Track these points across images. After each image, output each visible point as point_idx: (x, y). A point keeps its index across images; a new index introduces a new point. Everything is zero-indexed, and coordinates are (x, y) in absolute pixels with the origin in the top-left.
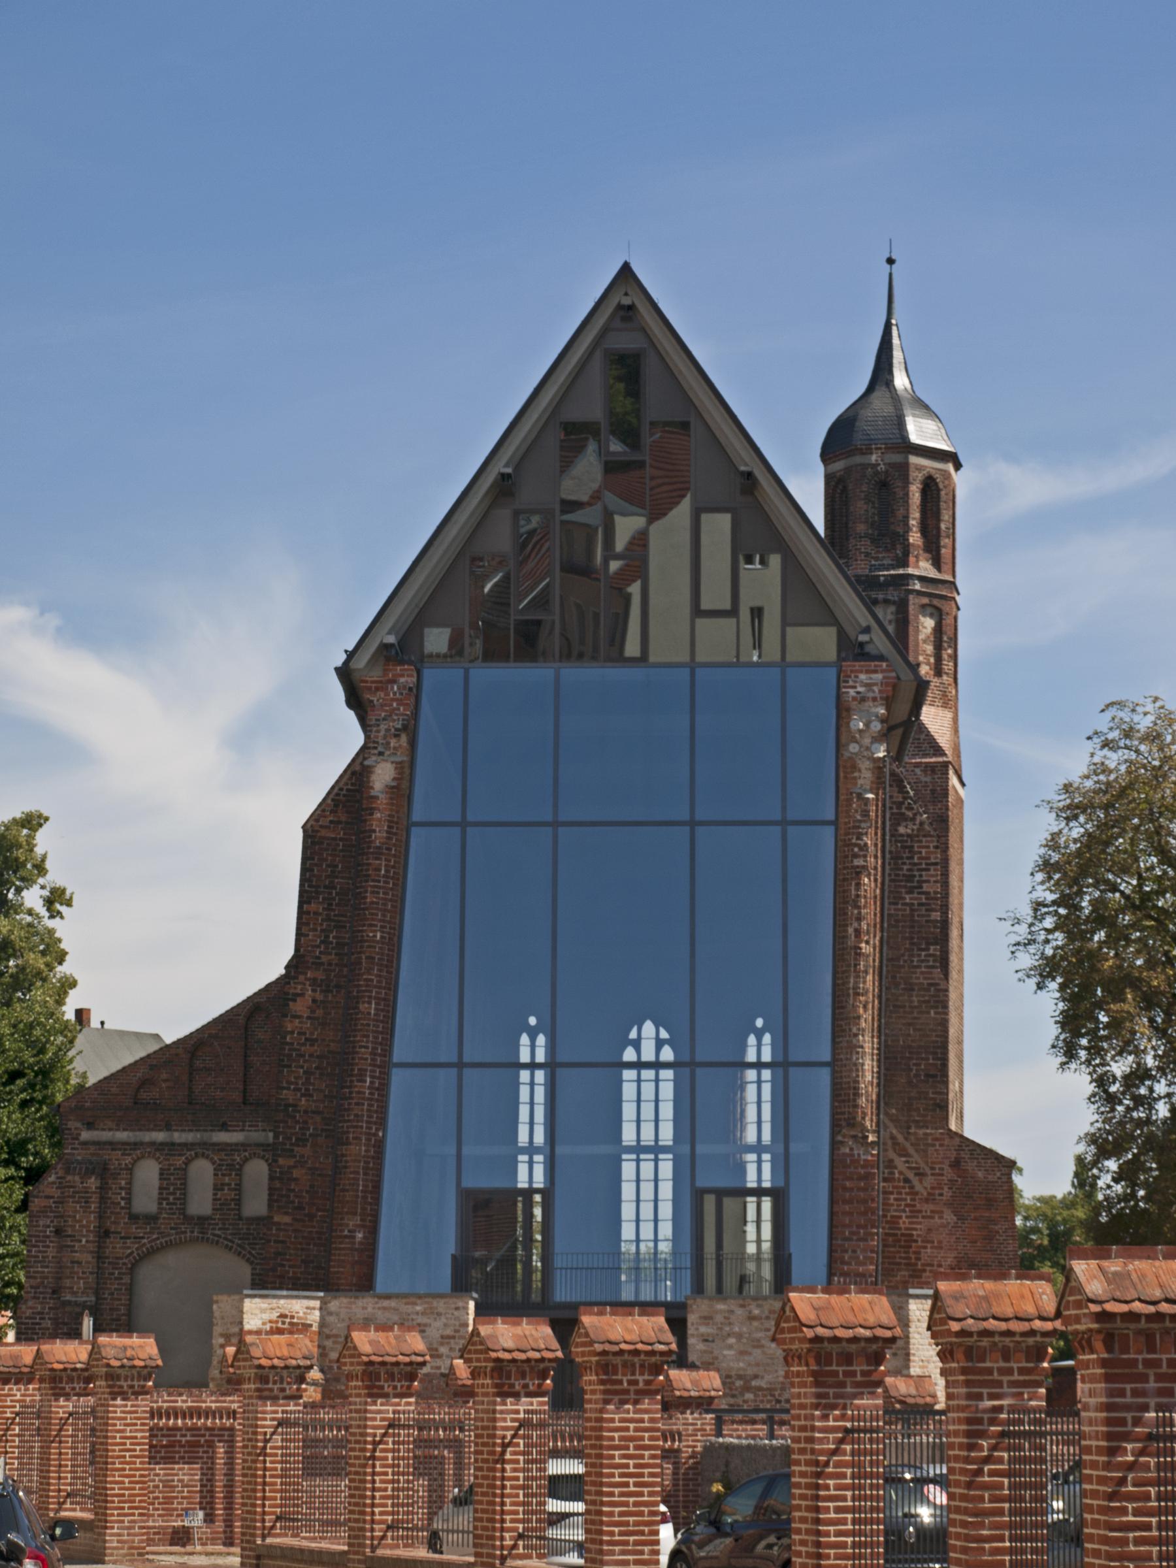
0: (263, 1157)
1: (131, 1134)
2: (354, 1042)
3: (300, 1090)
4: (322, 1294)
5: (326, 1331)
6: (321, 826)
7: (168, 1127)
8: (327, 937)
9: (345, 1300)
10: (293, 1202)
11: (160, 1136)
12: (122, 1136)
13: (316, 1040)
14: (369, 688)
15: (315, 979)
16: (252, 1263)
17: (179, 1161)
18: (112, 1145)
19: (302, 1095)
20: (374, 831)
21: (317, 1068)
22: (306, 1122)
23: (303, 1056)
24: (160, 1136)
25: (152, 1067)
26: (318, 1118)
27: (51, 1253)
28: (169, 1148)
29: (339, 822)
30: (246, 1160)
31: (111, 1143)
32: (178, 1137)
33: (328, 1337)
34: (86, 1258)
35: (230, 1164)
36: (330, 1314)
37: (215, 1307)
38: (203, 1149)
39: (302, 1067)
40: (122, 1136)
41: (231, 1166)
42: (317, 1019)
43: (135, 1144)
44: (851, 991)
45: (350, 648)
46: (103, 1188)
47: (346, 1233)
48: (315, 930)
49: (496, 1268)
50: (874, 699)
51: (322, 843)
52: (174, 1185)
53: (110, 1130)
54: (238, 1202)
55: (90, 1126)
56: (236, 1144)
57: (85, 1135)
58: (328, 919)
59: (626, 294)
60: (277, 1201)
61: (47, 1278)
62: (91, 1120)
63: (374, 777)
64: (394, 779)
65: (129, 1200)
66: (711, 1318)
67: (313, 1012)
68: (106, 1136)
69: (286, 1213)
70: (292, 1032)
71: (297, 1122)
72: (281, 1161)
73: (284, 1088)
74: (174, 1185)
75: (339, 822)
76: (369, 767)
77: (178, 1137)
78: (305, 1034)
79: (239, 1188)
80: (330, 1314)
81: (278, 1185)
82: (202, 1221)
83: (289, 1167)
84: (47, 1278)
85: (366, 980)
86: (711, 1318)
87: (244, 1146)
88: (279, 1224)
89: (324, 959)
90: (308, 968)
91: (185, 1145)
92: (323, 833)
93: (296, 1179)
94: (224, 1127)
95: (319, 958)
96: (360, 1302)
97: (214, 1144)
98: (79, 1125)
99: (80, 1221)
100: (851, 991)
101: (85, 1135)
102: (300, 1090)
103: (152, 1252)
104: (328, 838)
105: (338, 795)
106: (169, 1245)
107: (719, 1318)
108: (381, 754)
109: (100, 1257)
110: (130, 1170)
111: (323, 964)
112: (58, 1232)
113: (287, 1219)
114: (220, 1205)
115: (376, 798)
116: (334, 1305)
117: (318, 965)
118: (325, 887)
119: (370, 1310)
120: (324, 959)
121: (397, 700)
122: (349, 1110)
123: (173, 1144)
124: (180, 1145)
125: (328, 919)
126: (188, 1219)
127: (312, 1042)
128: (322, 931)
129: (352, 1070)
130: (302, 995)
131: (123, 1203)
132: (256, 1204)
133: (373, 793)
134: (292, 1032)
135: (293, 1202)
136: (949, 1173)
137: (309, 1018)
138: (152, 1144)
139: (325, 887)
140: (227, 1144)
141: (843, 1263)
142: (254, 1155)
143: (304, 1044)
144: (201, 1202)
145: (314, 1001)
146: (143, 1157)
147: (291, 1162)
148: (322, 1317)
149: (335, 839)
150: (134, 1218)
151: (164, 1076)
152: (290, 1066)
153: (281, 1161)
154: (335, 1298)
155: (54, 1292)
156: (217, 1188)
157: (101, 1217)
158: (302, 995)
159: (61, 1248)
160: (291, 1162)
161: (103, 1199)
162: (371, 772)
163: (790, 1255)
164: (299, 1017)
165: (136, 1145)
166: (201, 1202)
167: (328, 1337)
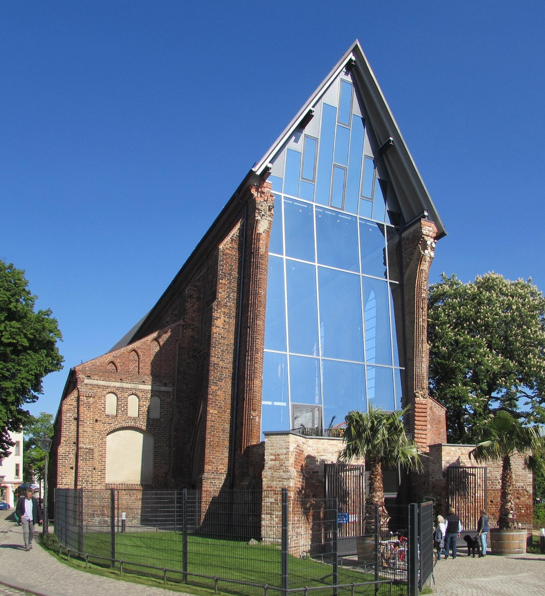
0: (158, 396)
3: (219, 358)
6: (226, 248)
11: (118, 384)
15: (225, 312)
18: (99, 386)
22: (222, 372)
23: (221, 344)
26: (227, 370)
29: (233, 248)
32: (125, 385)
39: (220, 348)
42: (226, 329)
48: (224, 291)
52: (122, 406)
61: (71, 437)
62: (89, 375)
64: (268, 228)
66: (449, 454)
71: (219, 371)
74: (122, 406)
75: (233, 248)
77: (125, 385)
84: (71, 437)
86: (449, 454)
88: (212, 413)
90: (223, 307)
92: (227, 251)
93: (219, 395)
98: (84, 377)
101: (87, 381)
102: (219, 358)
105: (233, 236)
107: (452, 453)
111: (228, 306)
113: (216, 412)
117: (225, 306)
120: (228, 304)
123: (123, 388)
124: (126, 388)
130: (220, 318)
134: (216, 333)
135: (217, 405)
137: (222, 328)
145: (224, 321)
150: (108, 416)
151: (119, 361)
158: (220, 318)
163: (14, 501)
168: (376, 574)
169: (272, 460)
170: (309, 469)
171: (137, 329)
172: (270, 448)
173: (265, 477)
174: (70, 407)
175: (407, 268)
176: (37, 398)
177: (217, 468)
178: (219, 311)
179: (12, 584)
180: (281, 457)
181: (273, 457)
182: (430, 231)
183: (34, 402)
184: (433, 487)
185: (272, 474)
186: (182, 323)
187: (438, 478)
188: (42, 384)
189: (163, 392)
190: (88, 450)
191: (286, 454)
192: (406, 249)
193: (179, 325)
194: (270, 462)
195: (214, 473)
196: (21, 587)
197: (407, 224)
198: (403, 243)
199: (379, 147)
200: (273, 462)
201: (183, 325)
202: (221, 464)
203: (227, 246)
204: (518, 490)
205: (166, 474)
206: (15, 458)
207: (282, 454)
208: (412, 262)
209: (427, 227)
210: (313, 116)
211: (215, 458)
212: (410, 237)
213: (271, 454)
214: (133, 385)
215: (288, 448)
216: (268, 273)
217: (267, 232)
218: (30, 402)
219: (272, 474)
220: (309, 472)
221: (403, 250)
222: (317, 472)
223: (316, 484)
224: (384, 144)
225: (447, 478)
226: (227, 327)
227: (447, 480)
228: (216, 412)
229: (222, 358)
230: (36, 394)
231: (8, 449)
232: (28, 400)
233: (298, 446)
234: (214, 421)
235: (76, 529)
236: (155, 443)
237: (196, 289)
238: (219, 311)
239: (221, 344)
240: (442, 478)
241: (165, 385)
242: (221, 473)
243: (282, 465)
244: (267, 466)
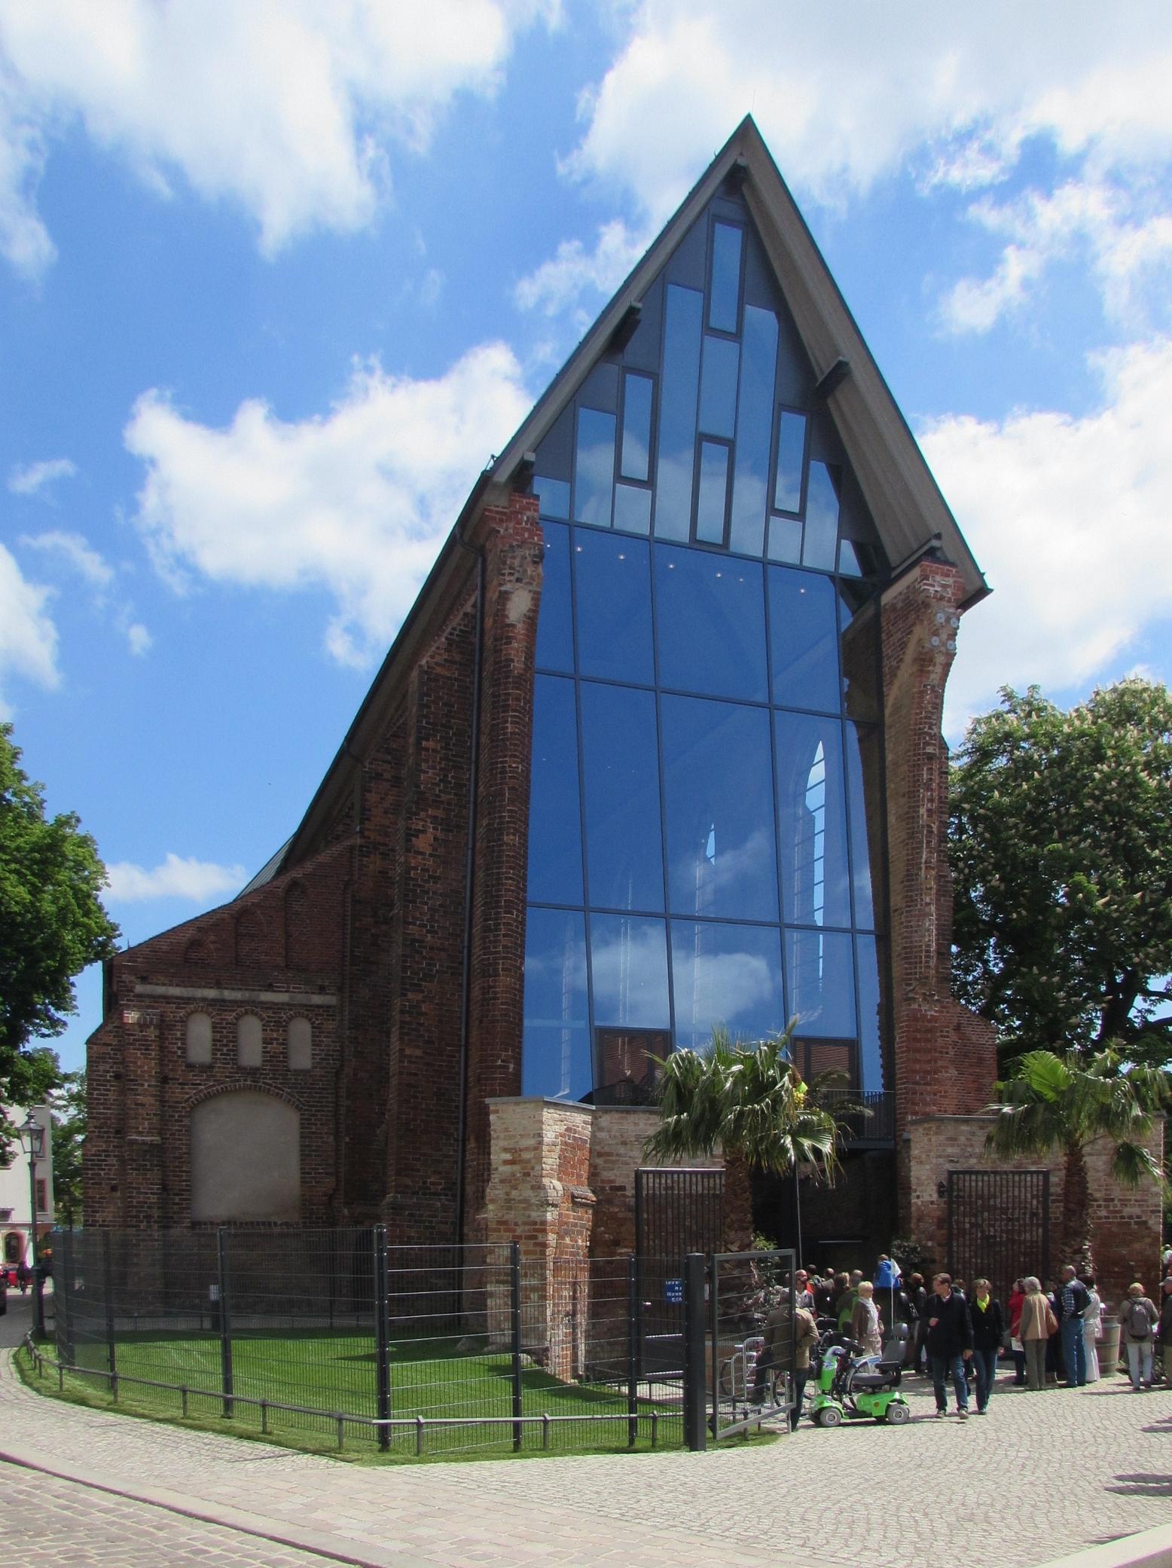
0: (307, 1017)
1: (183, 990)
2: (498, 874)
4: (594, 1107)
5: (598, 1148)
6: (436, 664)
7: (218, 985)
8: (446, 776)
9: (617, 1116)
10: (422, 1036)
11: (211, 993)
12: (175, 991)
13: (439, 878)
14: (494, 519)
15: (435, 817)
16: (300, 1109)
17: (230, 1017)
19: (428, 932)
20: (512, 661)
21: (441, 906)
23: (427, 892)
24: (211, 993)
25: (200, 929)
26: (443, 954)
27: (112, 1096)
28: (220, 1004)
29: (455, 663)
30: (291, 1018)
31: (165, 997)
32: (228, 994)
33: (600, 1155)
34: (149, 1100)
35: (276, 1021)
36: (601, 1129)
37: (492, 1117)
38: (252, 1007)
39: (426, 903)
40: (175, 991)
41: (278, 1023)
43: (189, 999)
44: (923, 866)
45: (497, 454)
46: (161, 1037)
47: (499, 1063)
48: (434, 768)
49: (734, 1084)
50: (949, 601)
51: (437, 680)
52: (226, 1040)
53: (164, 985)
54: (286, 1055)
55: (144, 980)
56: (283, 1004)
57: (139, 988)
58: (445, 758)
59: (741, 154)
60: (408, 1034)
63: (510, 605)
64: (530, 610)
65: (184, 1050)
66: (955, 1139)
67: (435, 849)
68: (160, 990)
69: (417, 1047)
70: (416, 868)
71: (424, 958)
72: (410, 995)
73: (410, 923)
74: (226, 1040)
75: (455, 663)
76: (506, 592)
77: (228, 994)
78: (427, 870)
79: (285, 1043)
80: (601, 1129)
81: (408, 1019)
82: (253, 1072)
83: (418, 1002)
85: (510, 811)
86: (955, 1139)
87: (289, 1006)
89: (444, 797)
91: (235, 1002)
92: (439, 670)
94: (270, 988)
95: (438, 796)
96: (632, 1118)
97: (262, 1003)
98: (133, 978)
99: (141, 1067)
100: (923, 866)
101: (139, 988)
103: (209, 1097)
104: (443, 677)
105: (451, 634)
106: (225, 1092)
107: (962, 1139)
108: (518, 580)
109: (162, 1102)
110: (184, 1022)
111: (442, 802)
112: (118, 1077)
113: (418, 1052)
114: (270, 1058)
115: (513, 626)
116: (605, 1120)
118: (443, 726)
119: (642, 1125)
120: (444, 797)
121: (528, 530)
122: (496, 941)
123: (224, 1001)
125: (445, 758)
126: (241, 1069)
127: (436, 879)
128: (441, 769)
129: (497, 902)
130: (424, 832)
131: (179, 1052)
132: (302, 1057)
133: (508, 621)
134: (416, 868)
136: (953, 1036)
138: (204, 999)
139: (443, 726)
140: (277, 1004)
141: (913, 1104)
142: (298, 1015)
143: (428, 881)
144: (252, 1053)
145: (435, 839)
146: (196, 1011)
147: (420, 997)
148: (593, 1133)
149: (449, 678)
150: (190, 1066)
151: (212, 938)
152: (414, 902)
153: (410, 995)
154: (606, 1112)
155: (117, 1132)
156: (266, 1042)
157: (161, 1063)
159: (122, 1092)
160: (420, 997)
161: (162, 1048)
162: (508, 599)
164: (422, 853)
165: (189, 1000)
166: (252, 1053)
167: (600, 1155)
168: (110, 1326)
169: (506, 1162)
170: (603, 1181)
171: (282, 856)
172: (502, 1135)
173: (492, 1201)
174: (104, 1049)
175: (891, 683)
176: (65, 1024)
177: (425, 1183)
178: (422, 814)
179: (243, 1526)
180: (526, 1156)
181: (508, 1156)
182: (944, 586)
183: (58, 1034)
184: (919, 1220)
185: (507, 1194)
186: (359, 841)
187: (927, 1198)
188: (74, 991)
189: (318, 1007)
190: (146, 1148)
191: (536, 1149)
192: (890, 635)
193: (352, 848)
194: (502, 1168)
195: (416, 1193)
196: (262, 1531)
197: (895, 568)
198: (883, 620)
199: (816, 379)
200: (507, 1168)
201: (361, 846)
202: (435, 1172)
203: (438, 659)
204: (1129, 1224)
205: (331, 1197)
206: (20, 1167)
207: (527, 1149)
208: (903, 666)
209: (938, 578)
210: (639, 321)
211: (418, 1159)
212: (899, 605)
213: (506, 1150)
214: (247, 994)
215: (540, 1135)
216: (535, 719)
217: (532, 620)
218: (48, 1036)
219: (507, 1194)
220: (603, 1189)
221: (884, 636)
222: (622, 1188)
223: (620, 1215)
224: (827, 371)
225: (950, 1196)
226: (441, 851)
227: (950, 1203)
228: (418, 1052)
229: (432, 926)
230: (60, 1015)
231: (9, 1145)
232: (45, 1031)
233: (568, 1129)
234: (416, 1075)
235: (710, 1411)
236: (302, 1126)
237: (389, 758)
238: (422, 814)
239: (427, 892)
240: (935, 1197)
241: (322, 990)
242: (435, 1194)
243: (528, 1174)
244: (495, 1178)
